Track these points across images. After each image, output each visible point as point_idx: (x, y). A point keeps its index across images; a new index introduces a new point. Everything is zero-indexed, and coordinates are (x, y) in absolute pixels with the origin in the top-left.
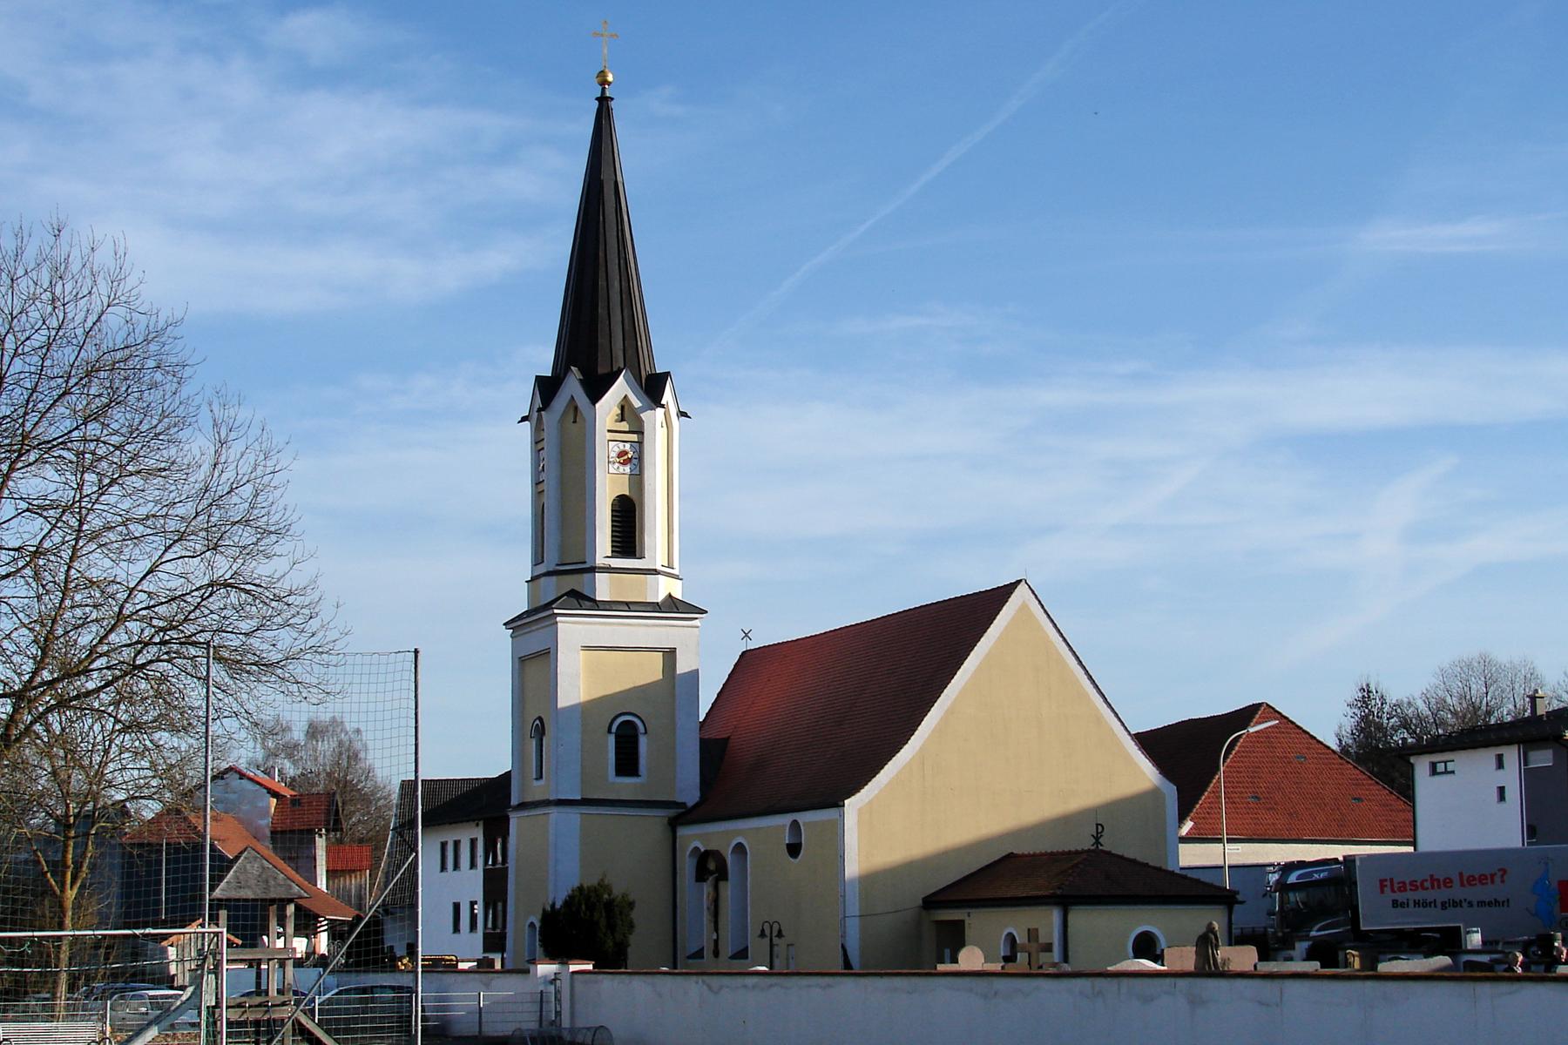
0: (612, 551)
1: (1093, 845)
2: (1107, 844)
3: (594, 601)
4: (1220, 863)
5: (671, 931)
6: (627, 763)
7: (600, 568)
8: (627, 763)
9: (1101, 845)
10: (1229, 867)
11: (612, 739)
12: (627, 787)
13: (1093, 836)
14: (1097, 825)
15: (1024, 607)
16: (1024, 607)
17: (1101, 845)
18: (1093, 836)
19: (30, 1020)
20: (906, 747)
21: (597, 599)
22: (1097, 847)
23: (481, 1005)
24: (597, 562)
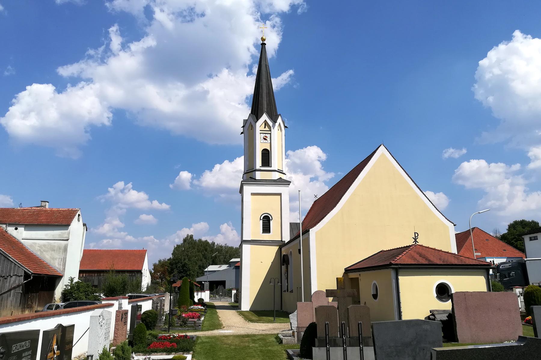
0: (262, 165)
1: (414, 242)
2: (421, 241)
3: (256, 179)
4: (273, 309)
5: (280, 304)
6: (266, 229)
7: (257, 170)
8: (266, 229)
9: (418, 242)
10: (276, 311)
11: (261, 221)
12: (266, 237)
13: (413, 238)
14: (415, 233)
15: (383, 155)
16: (383, 155)
17: (418, 242)
18: (413, 238)
19: (167, 342)
20: (53, 231)
21: (256, 179)
22: (416, 243)
23: (338, 310)
24: (257, 168)
